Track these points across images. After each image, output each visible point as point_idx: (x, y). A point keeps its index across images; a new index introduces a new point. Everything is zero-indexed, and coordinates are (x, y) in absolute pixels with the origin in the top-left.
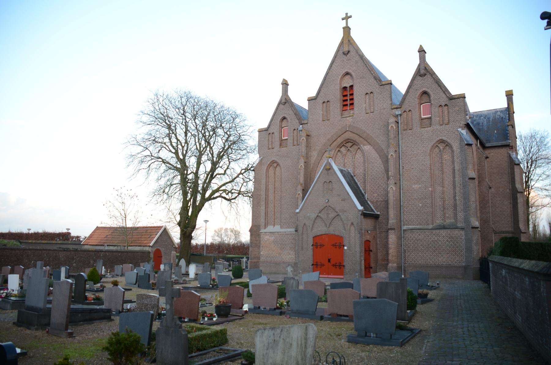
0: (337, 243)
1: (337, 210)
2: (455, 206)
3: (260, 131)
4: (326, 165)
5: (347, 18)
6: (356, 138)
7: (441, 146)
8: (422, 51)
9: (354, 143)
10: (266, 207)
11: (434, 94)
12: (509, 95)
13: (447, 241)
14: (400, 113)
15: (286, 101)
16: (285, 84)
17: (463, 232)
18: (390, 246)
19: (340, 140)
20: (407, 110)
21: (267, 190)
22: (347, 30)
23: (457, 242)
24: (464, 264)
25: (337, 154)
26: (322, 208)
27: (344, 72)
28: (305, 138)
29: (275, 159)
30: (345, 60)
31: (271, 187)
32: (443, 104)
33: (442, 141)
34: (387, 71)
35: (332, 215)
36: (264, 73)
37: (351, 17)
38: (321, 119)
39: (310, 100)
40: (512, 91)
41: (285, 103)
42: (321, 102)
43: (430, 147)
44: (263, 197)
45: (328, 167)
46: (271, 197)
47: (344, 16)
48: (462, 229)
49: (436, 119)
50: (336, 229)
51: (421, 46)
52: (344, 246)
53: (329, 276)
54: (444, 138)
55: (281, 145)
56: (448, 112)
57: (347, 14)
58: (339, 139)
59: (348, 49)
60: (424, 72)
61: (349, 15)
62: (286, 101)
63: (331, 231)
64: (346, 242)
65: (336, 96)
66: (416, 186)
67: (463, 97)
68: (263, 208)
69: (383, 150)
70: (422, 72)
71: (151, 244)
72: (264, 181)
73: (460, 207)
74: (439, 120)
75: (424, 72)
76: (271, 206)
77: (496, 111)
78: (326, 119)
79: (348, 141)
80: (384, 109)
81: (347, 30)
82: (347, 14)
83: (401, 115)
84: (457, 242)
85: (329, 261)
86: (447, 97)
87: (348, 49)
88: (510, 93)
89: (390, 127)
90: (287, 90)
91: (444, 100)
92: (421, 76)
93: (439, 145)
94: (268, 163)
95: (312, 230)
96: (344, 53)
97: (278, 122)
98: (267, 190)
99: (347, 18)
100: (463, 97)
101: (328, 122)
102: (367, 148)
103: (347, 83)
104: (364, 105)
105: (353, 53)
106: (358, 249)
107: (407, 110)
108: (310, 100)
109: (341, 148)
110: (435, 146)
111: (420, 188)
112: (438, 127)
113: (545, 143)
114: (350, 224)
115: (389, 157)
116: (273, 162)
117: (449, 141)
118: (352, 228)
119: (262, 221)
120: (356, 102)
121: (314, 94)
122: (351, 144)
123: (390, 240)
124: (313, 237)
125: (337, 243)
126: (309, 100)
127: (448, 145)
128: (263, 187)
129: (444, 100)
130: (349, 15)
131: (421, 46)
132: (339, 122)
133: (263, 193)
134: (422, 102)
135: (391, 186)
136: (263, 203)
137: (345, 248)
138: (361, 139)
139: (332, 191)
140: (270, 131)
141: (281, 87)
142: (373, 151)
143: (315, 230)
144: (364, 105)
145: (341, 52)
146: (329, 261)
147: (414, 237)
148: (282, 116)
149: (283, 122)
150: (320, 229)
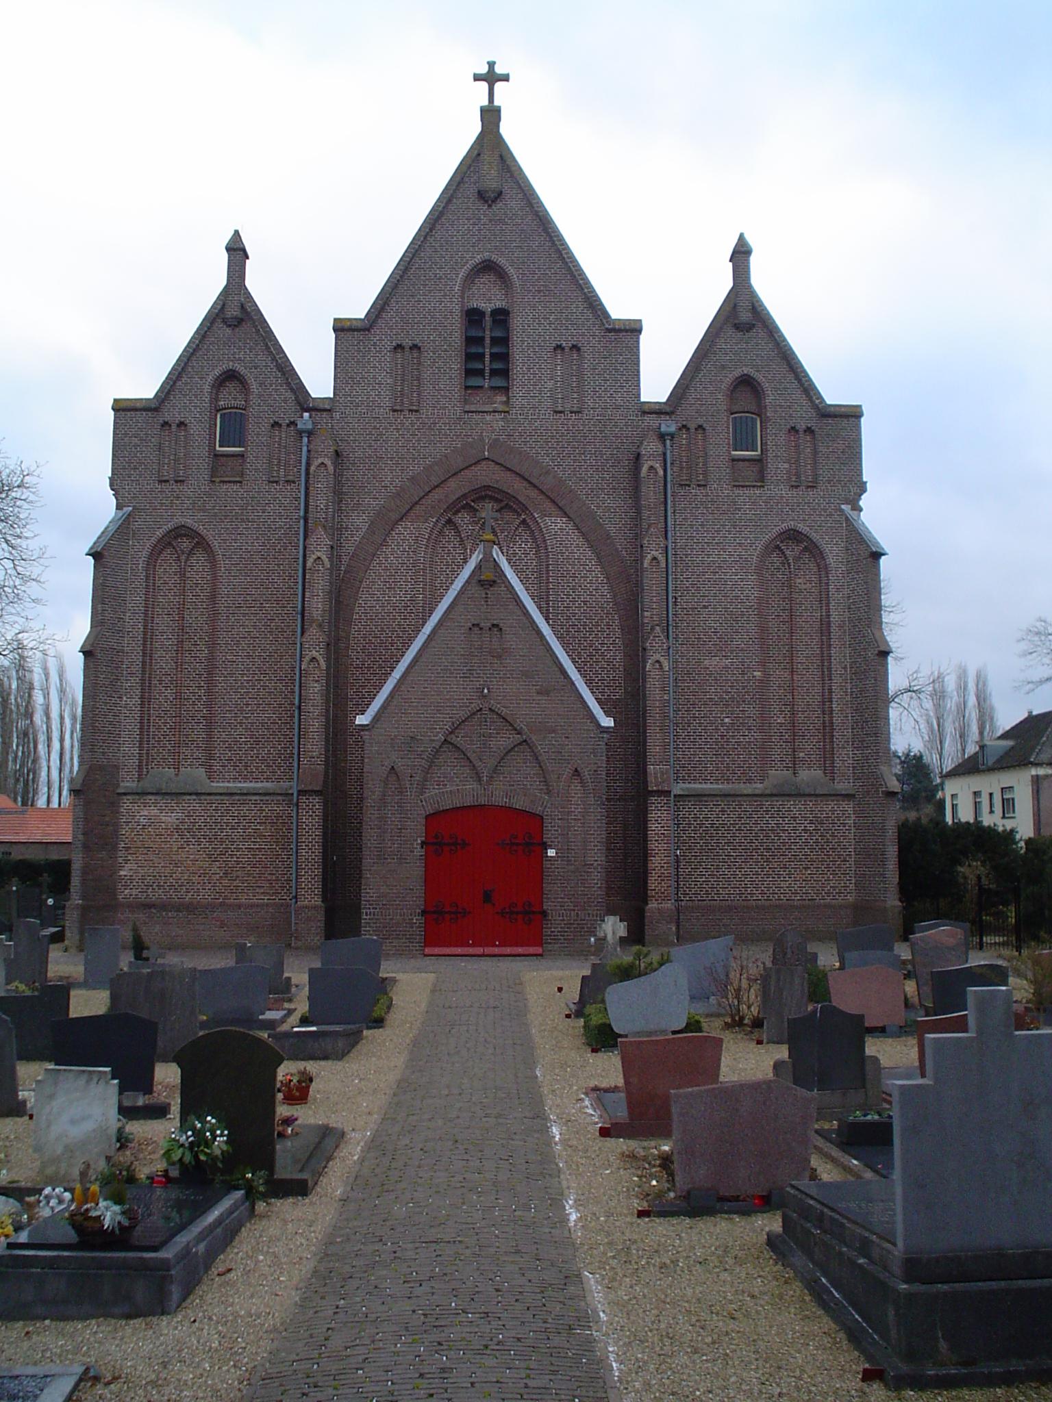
0: (521, 834)
1: (519, 724)
2: (827, 730)
3: (122, 408)
4: (479, 567)
6: (516, 487)
7: (792, 551)
8: (237, 251)
9: (506, 502)
10: (145, 700)
11: (776, 389)
13: (805, 830)
14: (673, 429)
15: (235, 318)
16: (741, 255)
17: (849, 807)
18: (652, 845)
19: (456, 488)
20: (692, 426)
21: (148, 636)
22: (491, 115)
23: (833, 835)
24: (851, 898)
25: (441, 532)
26: (463, 714)
27: (478, 258)
28: (328, 462)
29: (189, 522)
30: (484, 220)
31: (163, 623)
32: (801, 426)
33: (793, 536)
35: (505, 740)
38: (387, 402)
41: (240, 321)
42: (389, 344)
43: (760, 546)
44: (134, 658)
45: (488, 575)
46: (164, 661)
47: (484, 70)
48: (849, 797)
49: (778, 467)
50: (515, 788)
52: (545, 847)
53: (488, 950)
54: (801, 527)
55: (214, 472)
56: (815, 452)
57: (491, 65)
58: (452, 483)
62: (235, 318)
63: (498, 794)
64: (551, 831)
66: (712, 663)
68: (131, 701)
69: (608, 536)
70: (745, 316)
72: (136, 601)
73: (844, 733)
74: (789, 472)
76: (164, 696)
78: (405, 404)
79: (485, 493)
80: (617, 408)
81: (491, 115)
83: (672, 436)
84: (833, 835)
85: (487, 897)
87: (488, 184)
89: (644, 469)
92: (737, 327)
94: (159, 533)
95: (422, 789)
96: (481, 195)
97: (207, 388)
98: (148, 636)
99: (491, 77)
101: (413, 416)
102: (555, 525)
103: (488, 298)
104: (550, 384)
105: (512, 203)
106: (597, 856)
107: (692, 426)
109: (456, 513)
110: (775, 547)
111: (726, 667)
112: (784, 491)
114: (567, 772)
115: (646, 564)
116: (180, 532)
117: (815, 536)
118: (576, 787)
119: (128, 750)
120: (519, 365)
121: (358, 309)
123: (653, 826)
124: (427, 817)
125: (521, 834)
127: (813, 550)
128: (133, 622)
132: (452, 425)
133: (132, 646)
134: (735, 408)
135: (657, 657)
136: (131, 683)
137: (551, 853)
138: (533, 493)
139: (499, 657)
140: (172, 414)
142: (575, 539)
143: (432, 791)
144: (550, 384)
145: (470, 190)
146: (487, 897)
147: (707, 819)
148: (225, 366)
149: (224, 393)
150: (455, 788)
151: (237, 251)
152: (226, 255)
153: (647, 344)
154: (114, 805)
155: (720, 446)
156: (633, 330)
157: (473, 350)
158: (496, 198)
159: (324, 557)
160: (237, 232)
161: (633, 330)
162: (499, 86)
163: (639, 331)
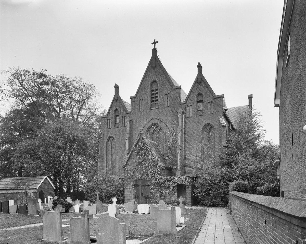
5: (155, 43)
12: (250, 98)
15: (117, 99)
22: (155, 51)
34: (186, 93)
36: (86, 80)
37: (157, 42)
39: (132, 98)
40: (252, 95)
51: (199, 63)
57: (155, 40)
59: (155, 64)
60: (200, 81)
61: (156, 41)
62: (117, 99)
65: (147, 97)
67: (222, 97)
71: (37, 188)
75: (200, 81)
77: (243, 107)
81: (155, 51)
82: (155, 40)
86: (213, 97)
88: (251, 96)
90: (118, 91)
91: (211, 99)
93: (207, 127)
99: (155, 43)
100: (222, 97)
108: (132, 98)
110: (205, 128)
113: (257, 123)
122: (156, 126)
126: (131, 98)
129: (211, 99)
130: (156, 41)
131: (199, 63)
141: (197, 69)
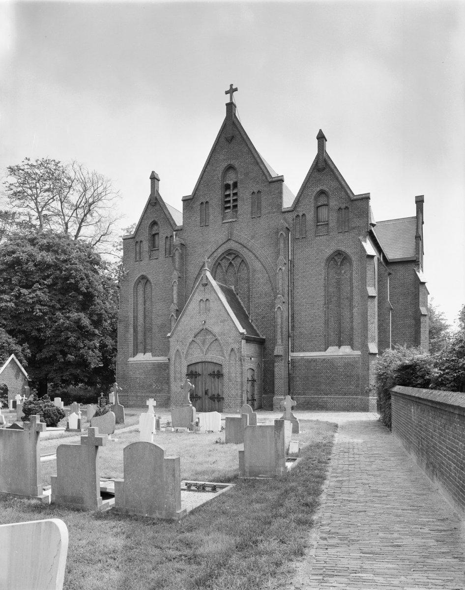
22: (231, 107)
26: (198, 331)
33: (339, 253)
47: (228, 89)
58: (219, 250)
81: (231, 107)
99: (232, 91)
121: (189, 192)
135: (279, 306)
143: (190, 358)
145: (222, 139)
151: (154, 178)
152: (317, 141)
153: (286, 183)
154: (273, 362)
155: (146, 246)
156: (280, 180)
157: (227, 199)
158: (232, 139)
159: (176, 281)
160: (320, 130)
161: (280, 180)
162: (235, 93)
163: (282, 181)
